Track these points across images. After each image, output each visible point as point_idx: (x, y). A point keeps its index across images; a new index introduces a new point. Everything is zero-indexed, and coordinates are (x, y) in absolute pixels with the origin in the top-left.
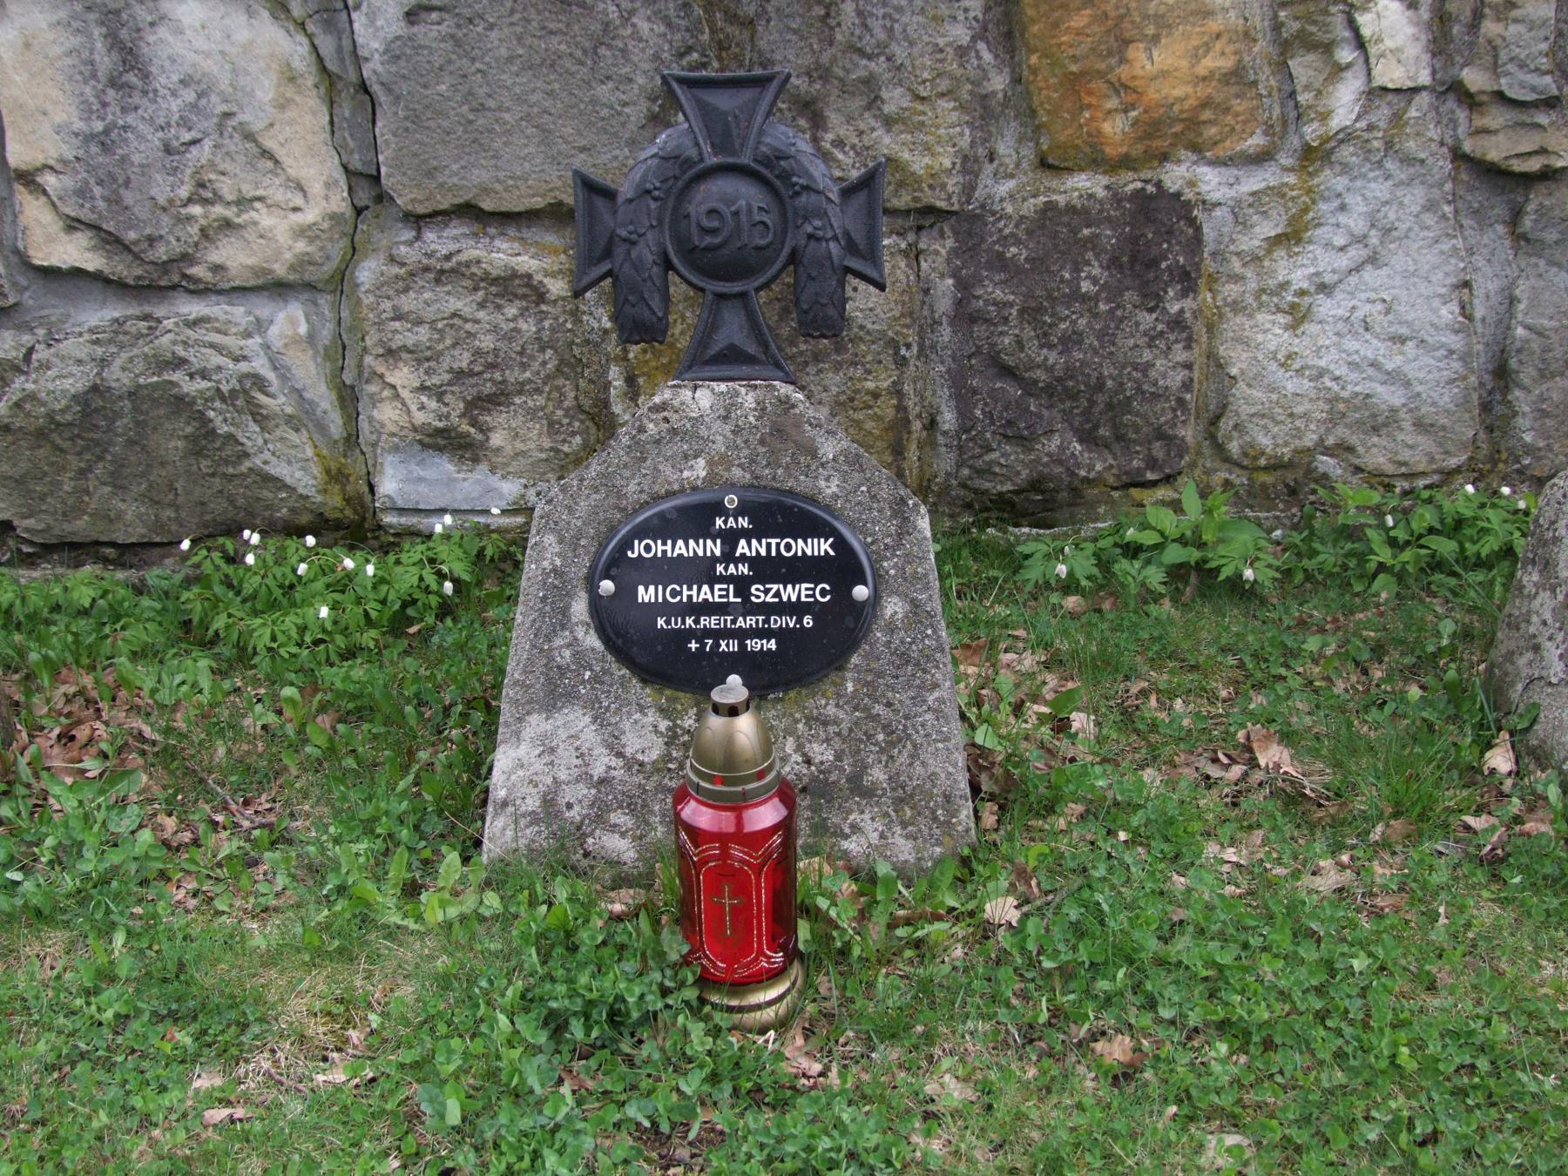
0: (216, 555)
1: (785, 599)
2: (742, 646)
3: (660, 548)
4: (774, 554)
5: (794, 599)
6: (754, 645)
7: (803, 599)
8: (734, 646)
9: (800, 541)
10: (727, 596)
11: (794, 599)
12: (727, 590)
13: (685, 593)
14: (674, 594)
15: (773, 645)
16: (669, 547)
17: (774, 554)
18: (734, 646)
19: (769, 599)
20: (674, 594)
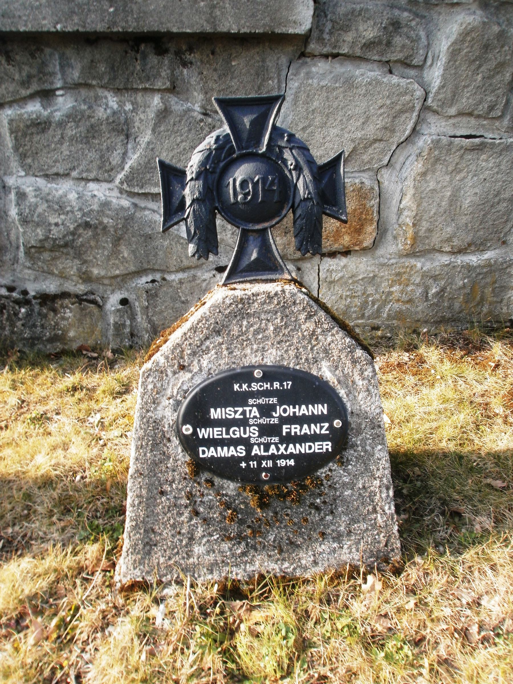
0: (445, 184)
1: (201, 437)
2: (275, 464)
3: (292, 410)
4: (242, 428)
5: (206, 437)
6: (282, 463)
7: (216, 437)
8: (270, 464)
9: (303, 452)
10: (222, 435)
11: (206, 437)
12: (222, 431)
13: (265, 386)
14: (261, 386)
15: (292, 462)
16: (297, 410)
17: (242, 428)
18: (270, 464)
19: (238, 416)
20: (261, 386)
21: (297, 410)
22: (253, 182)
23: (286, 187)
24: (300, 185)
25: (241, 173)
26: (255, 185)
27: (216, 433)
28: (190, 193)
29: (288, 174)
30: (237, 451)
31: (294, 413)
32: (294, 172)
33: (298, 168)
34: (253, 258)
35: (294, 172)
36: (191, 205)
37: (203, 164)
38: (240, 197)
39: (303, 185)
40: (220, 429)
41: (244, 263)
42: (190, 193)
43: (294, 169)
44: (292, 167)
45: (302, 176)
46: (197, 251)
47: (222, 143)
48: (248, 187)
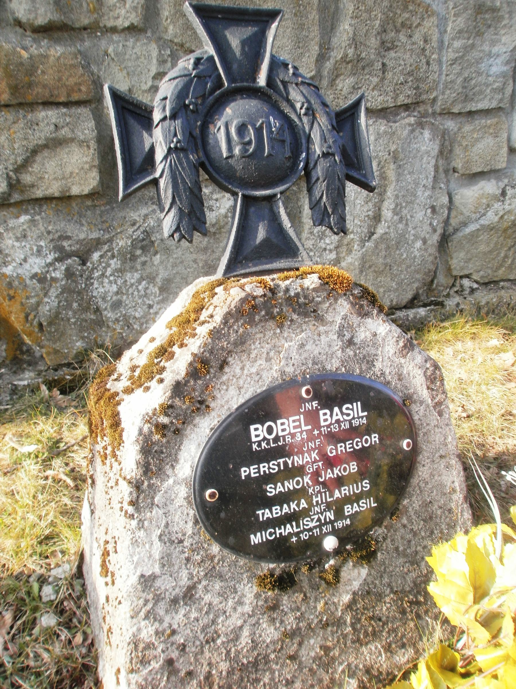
10: (300, 426)
12: (299, 420)
16: (282, 530)
21: (282, 530)
22: (254, 126)
23: (295, 139)
24: (316, 136)
25: (232, 113)
26: (259, 131)
27: (252, 471)
28: (158, 141)
29: (296, 120)
30: (342, 413)
31: (281, 534)
32: (305, 119)
33: (310, 112)
34: (258, 240)
35: (305, 119)
36: (165, 158)
37: (181, 95)
38: (237, 151)
39: (319, 137)
40: (297, 417)
41: (247, 250)
42: (158, 141)
43: (305, 114)
44: (303, 111)
45: (316, 125)
46: (178, 229)
47: (204, 67)
48: (249, 133)
